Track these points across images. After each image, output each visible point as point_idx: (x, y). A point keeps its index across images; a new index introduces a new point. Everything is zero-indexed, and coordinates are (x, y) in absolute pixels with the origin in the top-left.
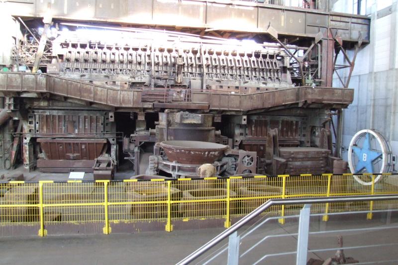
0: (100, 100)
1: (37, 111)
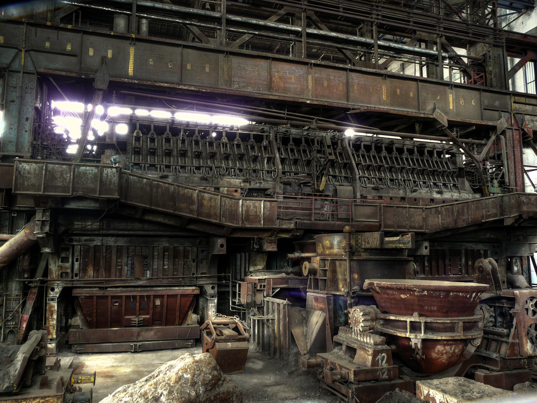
0: (209, 215)
1: (77, 238)
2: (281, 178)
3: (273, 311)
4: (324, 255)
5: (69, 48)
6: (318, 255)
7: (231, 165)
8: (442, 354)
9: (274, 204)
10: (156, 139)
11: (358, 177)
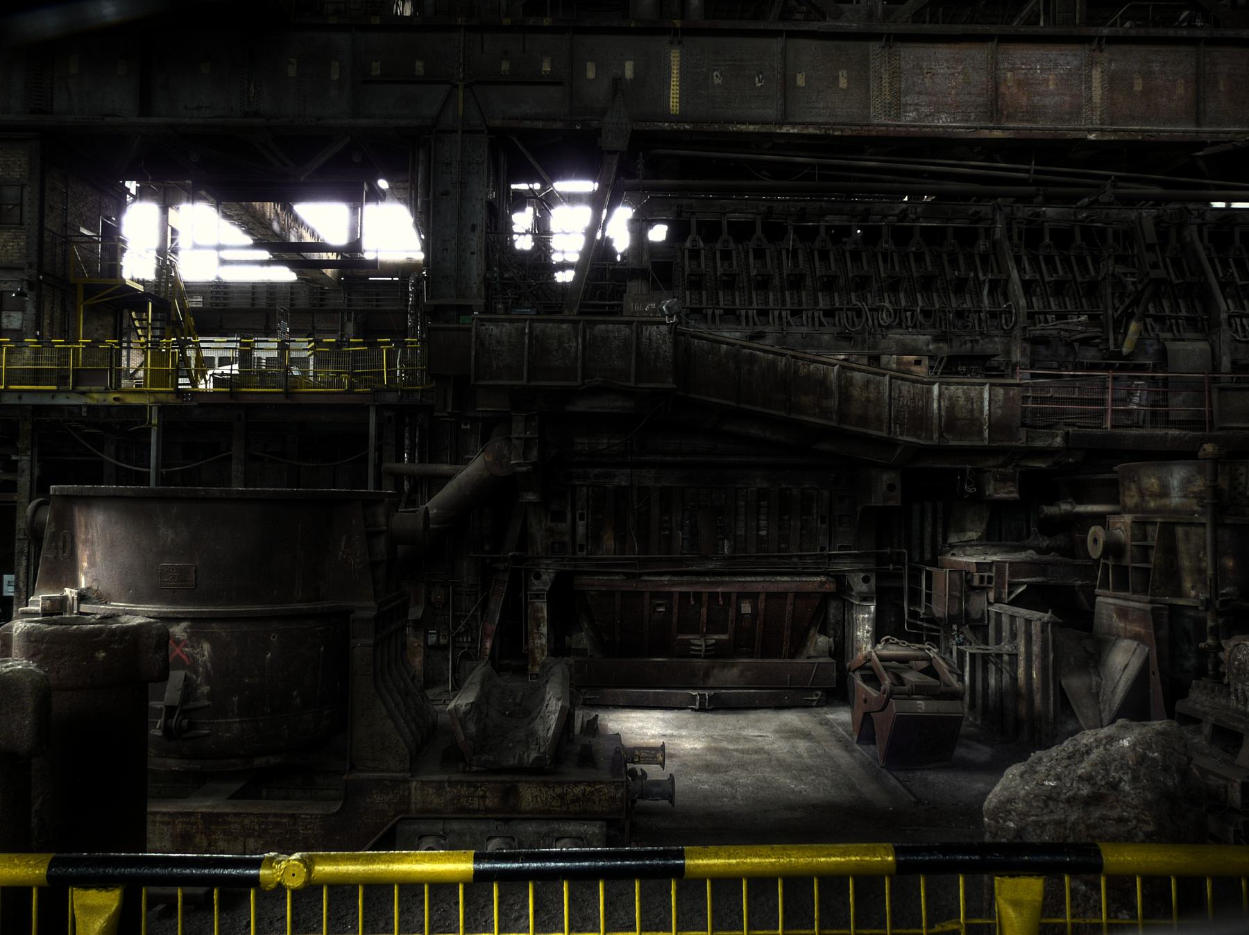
2: (1025, 328)
3: (1014, 636)
4: (1144, 511)
5: (546, 67)
6: (1125, 510)
7: (903, 304)
9: (1013, 392)
10: (734, 253)
11: (1224, 316)
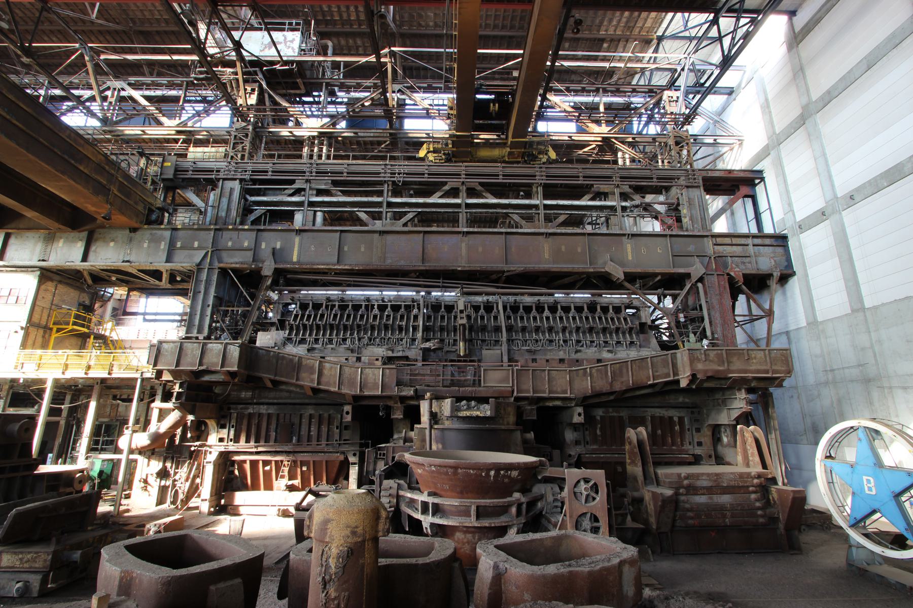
8: (464, 544)
